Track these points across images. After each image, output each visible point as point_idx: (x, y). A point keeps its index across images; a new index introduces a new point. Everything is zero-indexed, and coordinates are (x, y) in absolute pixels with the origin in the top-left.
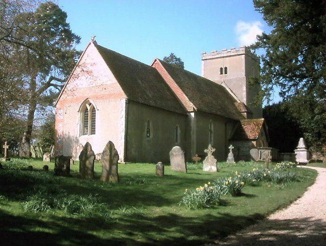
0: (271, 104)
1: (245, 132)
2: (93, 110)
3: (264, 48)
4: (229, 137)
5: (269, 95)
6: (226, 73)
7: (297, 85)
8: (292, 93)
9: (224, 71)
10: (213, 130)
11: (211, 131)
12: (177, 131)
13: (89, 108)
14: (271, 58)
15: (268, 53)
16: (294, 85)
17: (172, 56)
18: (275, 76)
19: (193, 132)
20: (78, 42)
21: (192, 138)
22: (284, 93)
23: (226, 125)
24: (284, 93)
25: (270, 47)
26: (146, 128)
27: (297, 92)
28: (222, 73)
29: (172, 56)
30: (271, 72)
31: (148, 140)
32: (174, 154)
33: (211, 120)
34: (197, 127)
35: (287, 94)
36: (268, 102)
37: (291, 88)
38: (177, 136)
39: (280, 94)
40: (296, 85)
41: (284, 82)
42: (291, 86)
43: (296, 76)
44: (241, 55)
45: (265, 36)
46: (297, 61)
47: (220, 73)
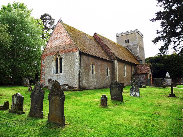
2: (61, 59)
4: (133, 73)
9: (127, 41)
12: (108, 70)
13: (58, 58)
23: (131, 66)
26: (91, 70)
28: (126, 42)
31: (92, 76)
38: (108, 72)
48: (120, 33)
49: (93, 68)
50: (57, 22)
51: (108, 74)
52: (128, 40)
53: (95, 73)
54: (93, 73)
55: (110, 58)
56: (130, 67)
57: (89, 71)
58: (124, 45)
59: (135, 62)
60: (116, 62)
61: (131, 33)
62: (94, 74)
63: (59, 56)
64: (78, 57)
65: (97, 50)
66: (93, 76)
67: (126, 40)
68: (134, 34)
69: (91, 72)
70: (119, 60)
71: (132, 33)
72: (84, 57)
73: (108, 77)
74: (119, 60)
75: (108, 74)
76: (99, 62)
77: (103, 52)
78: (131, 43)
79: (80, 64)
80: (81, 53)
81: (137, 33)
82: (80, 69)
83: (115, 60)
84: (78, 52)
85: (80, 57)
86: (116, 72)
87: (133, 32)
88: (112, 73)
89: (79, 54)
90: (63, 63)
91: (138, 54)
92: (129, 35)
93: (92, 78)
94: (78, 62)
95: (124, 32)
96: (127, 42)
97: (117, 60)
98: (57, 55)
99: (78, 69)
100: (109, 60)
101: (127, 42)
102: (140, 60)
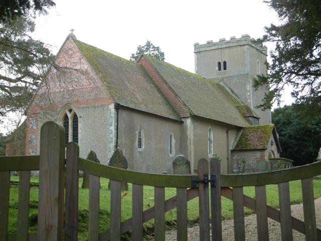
0: (282, 106)
1: (89, 202)
2: (75, 118)
3: (274, 41)
4: (231, 148)
5: (279, 95)
6: (225, 68)
7: (312, 84)
8: (306, 92)
9: (222, 66)
10: (212, 139)
11: (210, 141)
12: (171, 140)
13: (69, 115)
14: (280, 53)
15: (278, 47)
16: (308, 84)
17: (149, 45)
18: (286, 74)
19: (190, 142)
20: (32, 30)
21: (189, 148)
22: (297, 93)
23: (227, 132)
24: (297, 93)
25: (279, 40)
26: (137, 137)
27: (312, 91)
28: (220, 69)
29: (149, 45)
30: (282, 70)
31: (139, 152)
32: (178, 163)
33: (210, 127)
34: (195, 135)
35: (300, 93)
36: (279, 103)
37: (304, 87)
38: (171, 146)
39: (293, 94)
40: (310, 84)
41: (297, 80)
42: (305, 84)
43: (310, 73)
44: (244, 45)
45: (273, 28)
46: (312, 56)
47: (217, 68)
48: (205, 43)
49: (140, 136)
50: (65, 39)
51: (171, 148)
52: (225, 63)
53: (144, 146)
54: (140, 145)
55: (175, 112)
56: (225, 133)
57: (133, 143)
58: (213, 74)
59: (241, 122)
60: (189, 122)
61: (231, 45)
62: (143, 147)
63: (70, 111)
64: (113, 115)
65: (244, 123)
66: (140, 153)
67: (219, 63)
68: (239, 48)
69: (137, 143)
70: (196, 118)
71: (236, 44)
72: (124, 114)
73: (171, 155)
74: (196, 118)
75: (171, 148)
76: (154, 123)
77: (161, 100)
78: (231, 70)
79: (117, 129)
80: (118, 107)
81: (247, 47)
82: (117, 138)
83: (187, 117)
84: (114, 104)
85: (118, 114)
86: (190, 144)
87: (239, 41)
88: (181, 146)
89: (115, 108)
90: (80, 125)
91: (249, 101)
92: (227, 51)
93: (138, 155)
94: (113, 124)
95: (216, 40)
96: (222, 68)
97: (191, 118)
98: (65, 109)
99: (114, 139)
100: (172, 117)
101: (222, 68)
102: (251, 116)
